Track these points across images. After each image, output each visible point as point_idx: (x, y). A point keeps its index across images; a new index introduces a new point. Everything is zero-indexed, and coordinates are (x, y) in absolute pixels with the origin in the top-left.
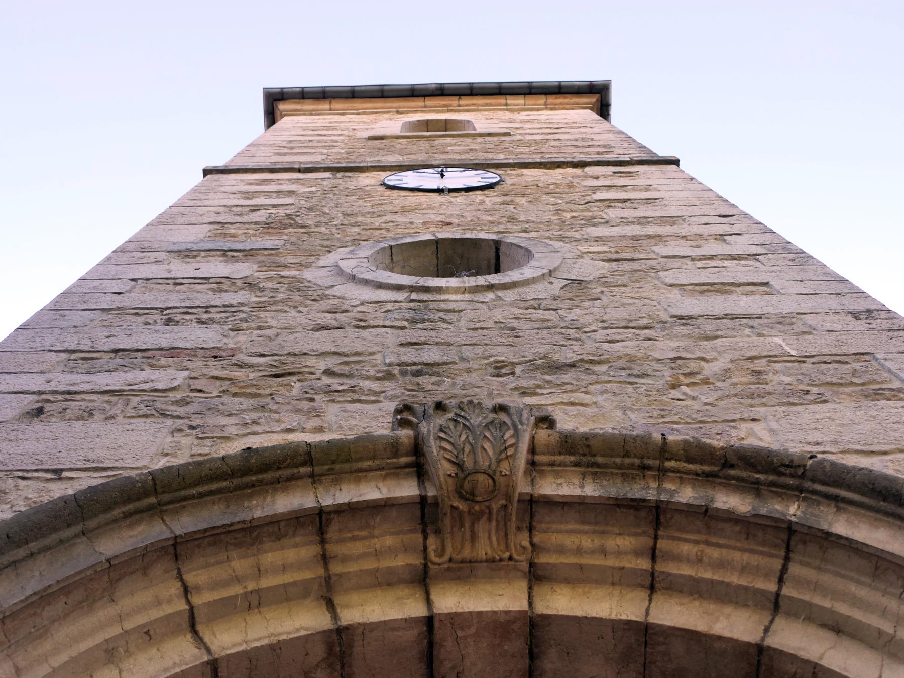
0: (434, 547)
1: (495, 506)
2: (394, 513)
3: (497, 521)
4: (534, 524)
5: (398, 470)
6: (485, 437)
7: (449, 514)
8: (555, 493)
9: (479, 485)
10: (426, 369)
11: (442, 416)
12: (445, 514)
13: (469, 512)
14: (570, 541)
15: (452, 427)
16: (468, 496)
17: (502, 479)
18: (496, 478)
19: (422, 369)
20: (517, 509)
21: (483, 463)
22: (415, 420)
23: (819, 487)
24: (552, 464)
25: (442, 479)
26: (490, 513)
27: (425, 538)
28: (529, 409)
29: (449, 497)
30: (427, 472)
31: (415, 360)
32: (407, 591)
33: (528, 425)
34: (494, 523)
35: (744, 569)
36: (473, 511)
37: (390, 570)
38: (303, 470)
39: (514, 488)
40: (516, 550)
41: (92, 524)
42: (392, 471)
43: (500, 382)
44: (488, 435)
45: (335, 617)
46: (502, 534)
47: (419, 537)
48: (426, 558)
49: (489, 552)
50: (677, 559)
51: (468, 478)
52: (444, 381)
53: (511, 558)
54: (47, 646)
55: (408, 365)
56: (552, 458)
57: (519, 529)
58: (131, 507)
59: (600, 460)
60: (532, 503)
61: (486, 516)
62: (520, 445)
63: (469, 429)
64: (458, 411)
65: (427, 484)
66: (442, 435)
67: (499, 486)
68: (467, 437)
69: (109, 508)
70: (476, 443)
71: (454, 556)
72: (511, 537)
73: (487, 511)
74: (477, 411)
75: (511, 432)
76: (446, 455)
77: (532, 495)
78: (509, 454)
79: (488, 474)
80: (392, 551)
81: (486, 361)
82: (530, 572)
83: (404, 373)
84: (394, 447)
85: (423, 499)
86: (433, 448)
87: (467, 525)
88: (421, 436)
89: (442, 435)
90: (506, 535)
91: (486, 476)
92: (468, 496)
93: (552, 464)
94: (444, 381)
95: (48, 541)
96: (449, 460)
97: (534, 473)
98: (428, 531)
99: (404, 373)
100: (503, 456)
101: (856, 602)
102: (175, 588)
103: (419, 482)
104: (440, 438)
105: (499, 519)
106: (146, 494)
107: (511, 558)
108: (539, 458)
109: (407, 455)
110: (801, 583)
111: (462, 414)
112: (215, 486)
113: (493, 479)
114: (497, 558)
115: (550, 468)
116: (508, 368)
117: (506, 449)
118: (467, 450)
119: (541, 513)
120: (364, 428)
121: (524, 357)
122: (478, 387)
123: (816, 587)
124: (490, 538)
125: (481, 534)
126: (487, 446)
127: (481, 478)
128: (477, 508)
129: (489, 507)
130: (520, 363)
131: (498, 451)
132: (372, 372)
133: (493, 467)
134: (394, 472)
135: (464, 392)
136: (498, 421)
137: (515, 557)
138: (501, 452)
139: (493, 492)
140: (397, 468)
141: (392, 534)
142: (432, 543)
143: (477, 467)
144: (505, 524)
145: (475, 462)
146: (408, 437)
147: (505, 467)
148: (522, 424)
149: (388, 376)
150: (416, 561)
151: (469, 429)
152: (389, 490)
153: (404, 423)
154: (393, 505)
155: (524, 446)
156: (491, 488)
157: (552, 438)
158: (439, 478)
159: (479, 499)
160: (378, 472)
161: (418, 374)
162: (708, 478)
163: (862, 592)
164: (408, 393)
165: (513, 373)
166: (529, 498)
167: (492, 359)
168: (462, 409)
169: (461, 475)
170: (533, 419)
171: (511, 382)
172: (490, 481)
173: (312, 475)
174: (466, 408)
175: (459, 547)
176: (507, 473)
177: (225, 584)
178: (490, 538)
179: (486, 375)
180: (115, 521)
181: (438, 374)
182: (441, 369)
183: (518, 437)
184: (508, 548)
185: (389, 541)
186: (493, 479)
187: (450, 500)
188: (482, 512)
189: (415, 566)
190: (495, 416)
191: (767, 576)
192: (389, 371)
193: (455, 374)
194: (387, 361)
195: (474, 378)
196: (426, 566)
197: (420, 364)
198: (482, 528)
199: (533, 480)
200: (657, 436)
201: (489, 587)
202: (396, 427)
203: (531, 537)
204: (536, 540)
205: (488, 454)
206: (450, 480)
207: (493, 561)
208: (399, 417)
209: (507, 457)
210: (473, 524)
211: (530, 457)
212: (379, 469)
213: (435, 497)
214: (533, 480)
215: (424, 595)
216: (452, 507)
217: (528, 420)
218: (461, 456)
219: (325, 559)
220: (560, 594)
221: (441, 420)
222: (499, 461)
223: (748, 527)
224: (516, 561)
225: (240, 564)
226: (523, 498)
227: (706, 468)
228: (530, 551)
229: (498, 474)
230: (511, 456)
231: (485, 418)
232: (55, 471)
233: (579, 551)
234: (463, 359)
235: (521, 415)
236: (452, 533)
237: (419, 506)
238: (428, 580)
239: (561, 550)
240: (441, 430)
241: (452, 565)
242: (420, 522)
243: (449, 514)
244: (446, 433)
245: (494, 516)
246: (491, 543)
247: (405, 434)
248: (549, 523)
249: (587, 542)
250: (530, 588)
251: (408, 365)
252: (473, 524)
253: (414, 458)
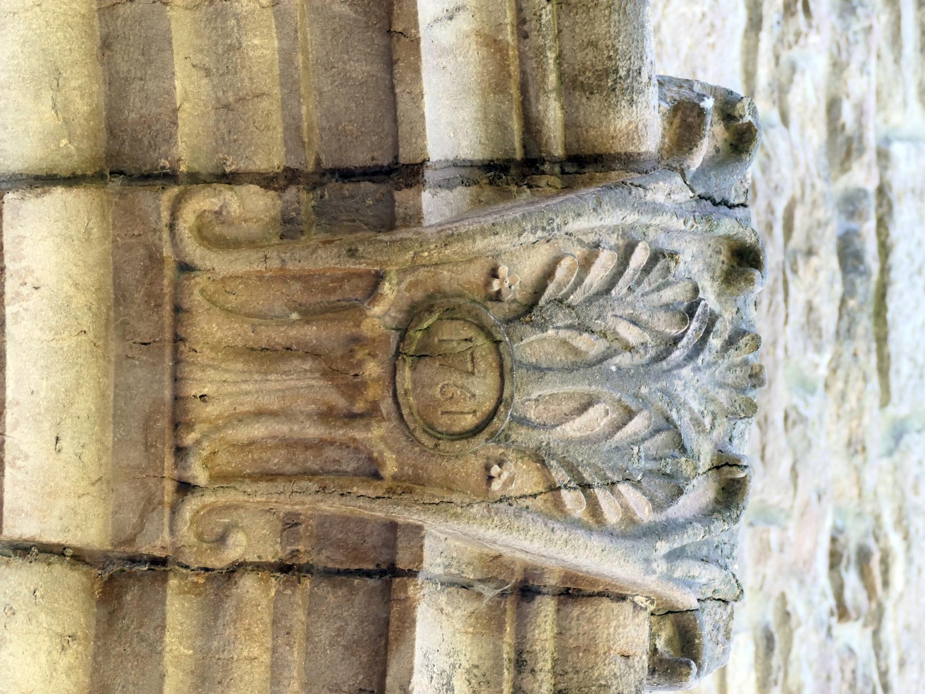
0: (235, 208)
1: (375, 436)
2: (362, 67)
3: (320, 445)
4: (307, 582)
5: (514, 91)
6: (630, 414)
7: (351, 265)
8: (418, 660)
9: (456, 377)
10: (867, 287)
11: (709, 267)
12: (352, 253)
13: (357, 340)
15: (668, 295)
16: (413, 341)
17: (475, 465)
18: (479, 442)
19: (866, 273)
20: (361, 521)
21: (534, 399)
22: (697, 159)
24: (521, 663)
25: (481, 244)
26: (351, 417)
27: (267, 181)
28: (725, 592)
29: (414, 267)
30: (506, 195)
31: (898, 256)
32: (81, 106)
33: (668, 578)
34: (313, 431)
36: (360, 355)
37: (155, 48)
39: (440, 507)
40: (214, 510)
42: (514, 69)
43: (808, 562)
44: (638, 424)
46: (276, 461)
47: (271, 156)
48: (195, 179)
49: (211, 410)
51: (481, 341)
52: (818, 349)
53: (185, 488)
55: (882, 225)
56: (545, 664)
57: (291, 524)
60: (381, 575)
61: (339, 402)
62: (597, 542)
63: (659, 358)
64: (723, 328)
65: (460, 196)
66: (640, 257)
67: (454, 450)
68: (630, 348)
70: (608, 377)
71: (200, 280)
72: (261, 494)
73: (359, 407)
74: (723, 396)
75: (645, 513)
76: (565, 263)
77: (412, 574)
78: (568, 496)
79: (494, 412)
80: (224, 58)
81: (888, 519)
82: (134, 560)
83: (851, 204)
84: (598, 80)
85: (410, 173)
86: (594, 216)
87: (311, 333)
88: (635, 177)
89: (640, 257)
90: (271, 476)
91: (488, 406)
92: (413, 341)
93: (521, 663)
94: (818, 349)
96: (548, 274)
97: (489, 592)
98: (292, 191)
99: (851, 204)
100: (560, 476)
103: (471, 165)
104: (629, 249)
105: (331, 453)
107: (185, 488)
108: (546, 609)
109: (569, 125)
111: (715, 342)
113: (476, 431)
114: (189, 439)
115: (507, 652)
116: (862, 596)
117: (585, 487)
118: (582, 342)
119: (347, 608)
120: (657, 29)
121: (902, 664)
122: (794, 471)
124: (260, 414)
125: (275, 382)
126: (597, 419)
127: (482, 389)
128: (372, 369)
129: (371, 413)
130: (877, 646)
131: (578, 455)
132: (857, 85)
133: (521, 435)
134: (511, 76)
135: (778, 417)
136: (687, 469)
137: (191, 506)
138: (572, 469)
139: (428, 430)
140: (524, 88)
141: (287, 58)
142: (251, 205)
143: (520, 373)
144: (309, 474)
145: (539, 370)
146: (634, 134)
147: (517, 477)
148: (674, 556)
149: (843, 147)
150: (187, 147)
151: (659, 358)
152: (445, 52)
153: (686, 119)
154: (390, 63)
155: (592, 557)
156: (443, 423)
157: (619, 666)
158: (483, 232)
159: (406, 377)
160: (509, 17)
161: (849, 255)
164: (780, 212)
165: (842, 612)
166: (403, 563)
167: (895, 541)
168: (730, 343)
169: (493, 315)
170: (686, 599)
171: (812, 600)
172: (469, 421)
174: (735, 357)
175: (232, 301)
176: (496, 486)
178: (260, 414)
179: (839, 512)
181: (845, 333)
182: (863, 343)
183: (624, 536)
184: (223, 479)
185: (262, 46)
186: (476, 431)
187: (404, 272)
188: (355, 388)
189: (170, 139)
190: (705, 462)
192: (861, 151)
193: (843, 397)
194: (898, 150)
195: (828, 465)
196: (169, 177)
197: (885, 270)
198: (301, 385)
199: (466, 586)
201: (86, 402)
202: (673, 92)
203: (258, 567)
204: (248, 585)
205: (567, 417)
206: (475, 273)
207: (178, 425)
208: (709, 103)
209: (554, 489)
210: (313, 353)
211: (552, 581)
212: (521, 22)
213: (415, 218)
214: (466, 586)
215: (64, 167)
216: (378, 278)
217: (688, 583)
218: (562, 318)
220: (53, 665)
221: (696, 262)
222: (539, 458)
224: (175, 510)
226: (402, 543)
228: (213, 562)
229: (497, 451)
230: (559, 504)
231: (697, 423)
234: (898, 434)
235: (705, 560)
236: (283, 277)
237: (385, 160)
238: (116, 184)
240: (656, 256)
241: (169, 271)
242: (327, 164)
243: (351, 265)
244: (647, 270)
245: (340, 433)
246: (242, 418)
247: (644, 123)
248: (308, 637)
250: (78, 557)
251: (882, 225)
252: (313, 353)
253: (558, 151)
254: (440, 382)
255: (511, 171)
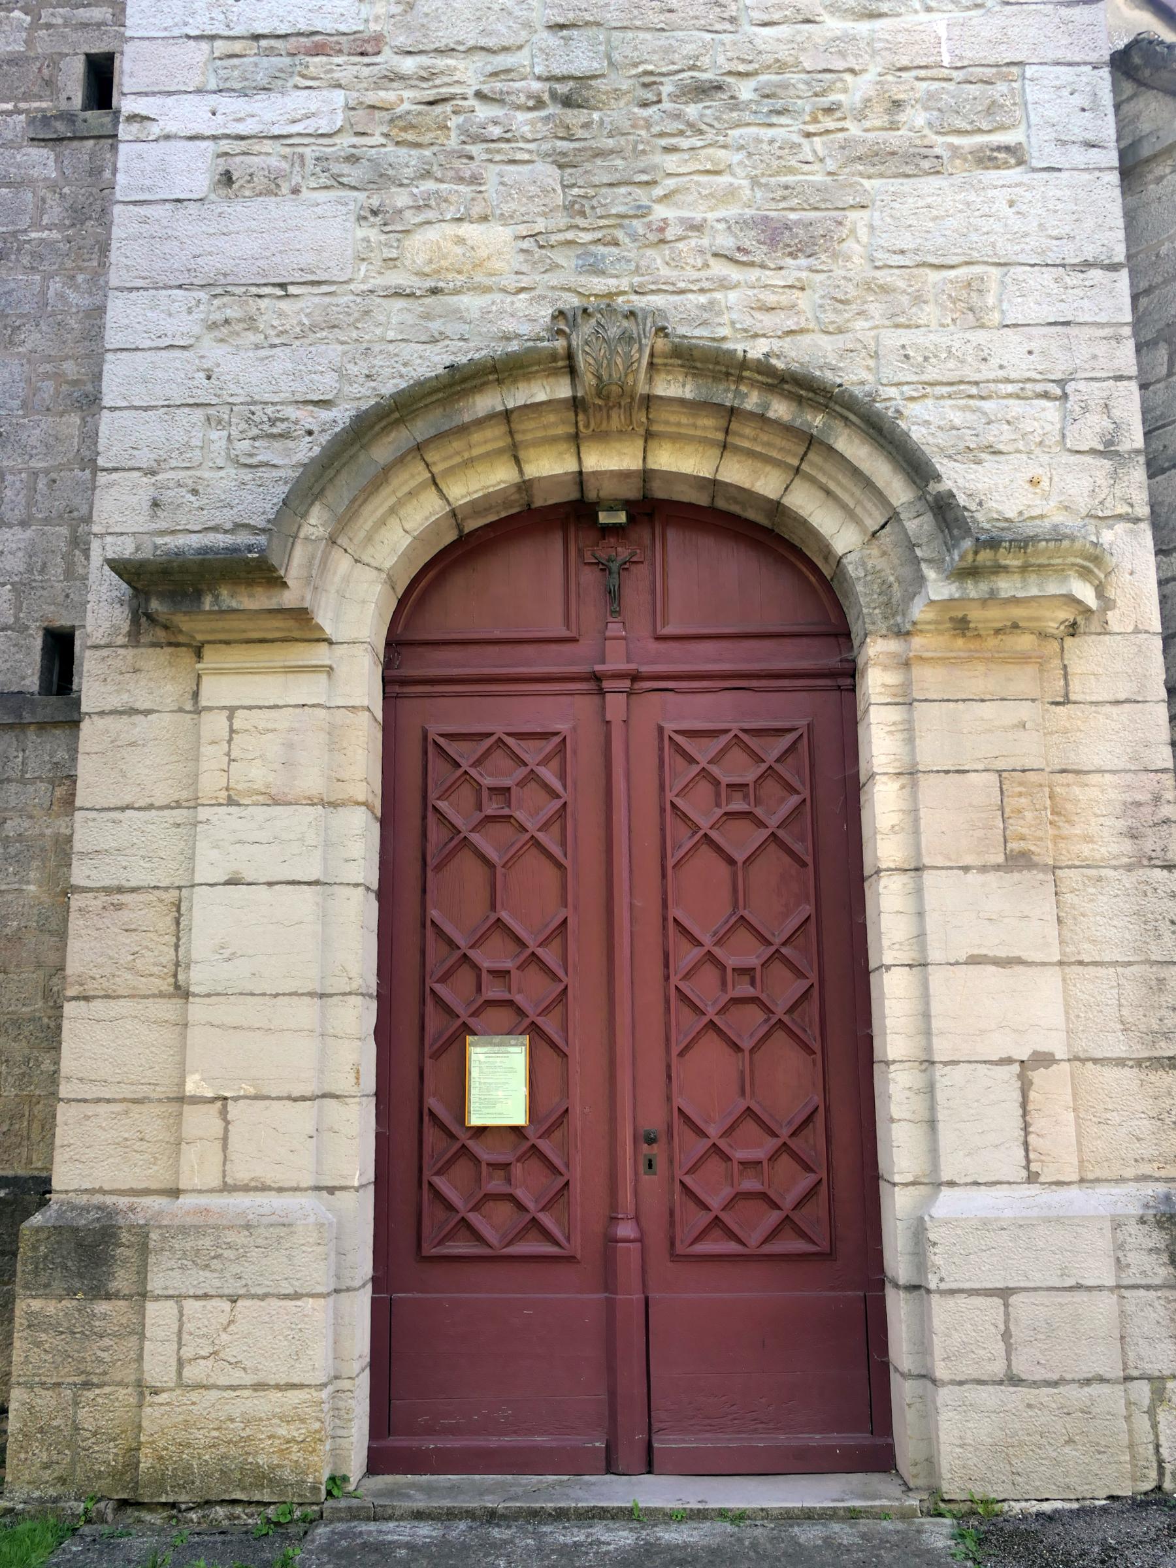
14: (673, 418)
23: (838, 408)
24: (665, 365)
35: (781, 449)
38: (491, 377)
41: (364, 441)
45: (521, 472)
47: (572, 414)
50: (742, 436)
54: (361, 520)
58: (384, 423)
59: (699, 365)
69: (372, 427)
75: (636, 346)
84: (553, 356)
85: (574, 398)
95: (344, 460)
101: (839, 483)
102: (421, 466)
106: (391, 412)
108: (656, 360)
110: (812, 464)
112: (434, 398)
123: (821, 469)
126: (619, 361)
150: (572, 430)
162: (770, 388)
163: (844, 481)
167: (640, 69)
173: (498, 380)
177: (450, 457)
180: (378, 434)
191: (794, 455)
198: (614, 414)
200: (740, 354)
219: (511, 433)
223: (787, 429)
225: (457, 445)
227: (770, 381)
232: (282, 286)
233: (679, 424)
239: (667, 423)
249: (684, 420)
254: (613, 394)
255: (572, 371)
